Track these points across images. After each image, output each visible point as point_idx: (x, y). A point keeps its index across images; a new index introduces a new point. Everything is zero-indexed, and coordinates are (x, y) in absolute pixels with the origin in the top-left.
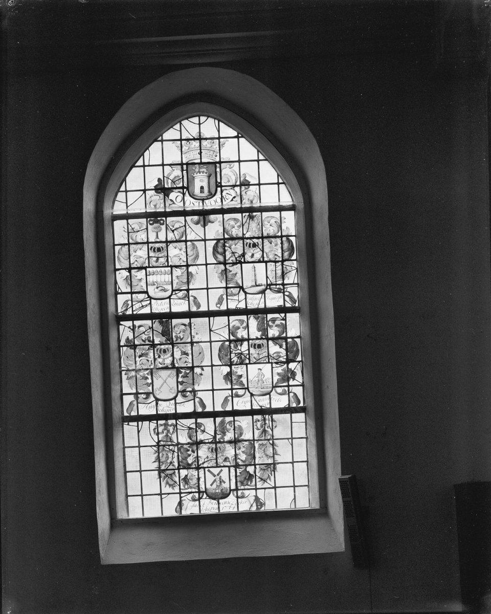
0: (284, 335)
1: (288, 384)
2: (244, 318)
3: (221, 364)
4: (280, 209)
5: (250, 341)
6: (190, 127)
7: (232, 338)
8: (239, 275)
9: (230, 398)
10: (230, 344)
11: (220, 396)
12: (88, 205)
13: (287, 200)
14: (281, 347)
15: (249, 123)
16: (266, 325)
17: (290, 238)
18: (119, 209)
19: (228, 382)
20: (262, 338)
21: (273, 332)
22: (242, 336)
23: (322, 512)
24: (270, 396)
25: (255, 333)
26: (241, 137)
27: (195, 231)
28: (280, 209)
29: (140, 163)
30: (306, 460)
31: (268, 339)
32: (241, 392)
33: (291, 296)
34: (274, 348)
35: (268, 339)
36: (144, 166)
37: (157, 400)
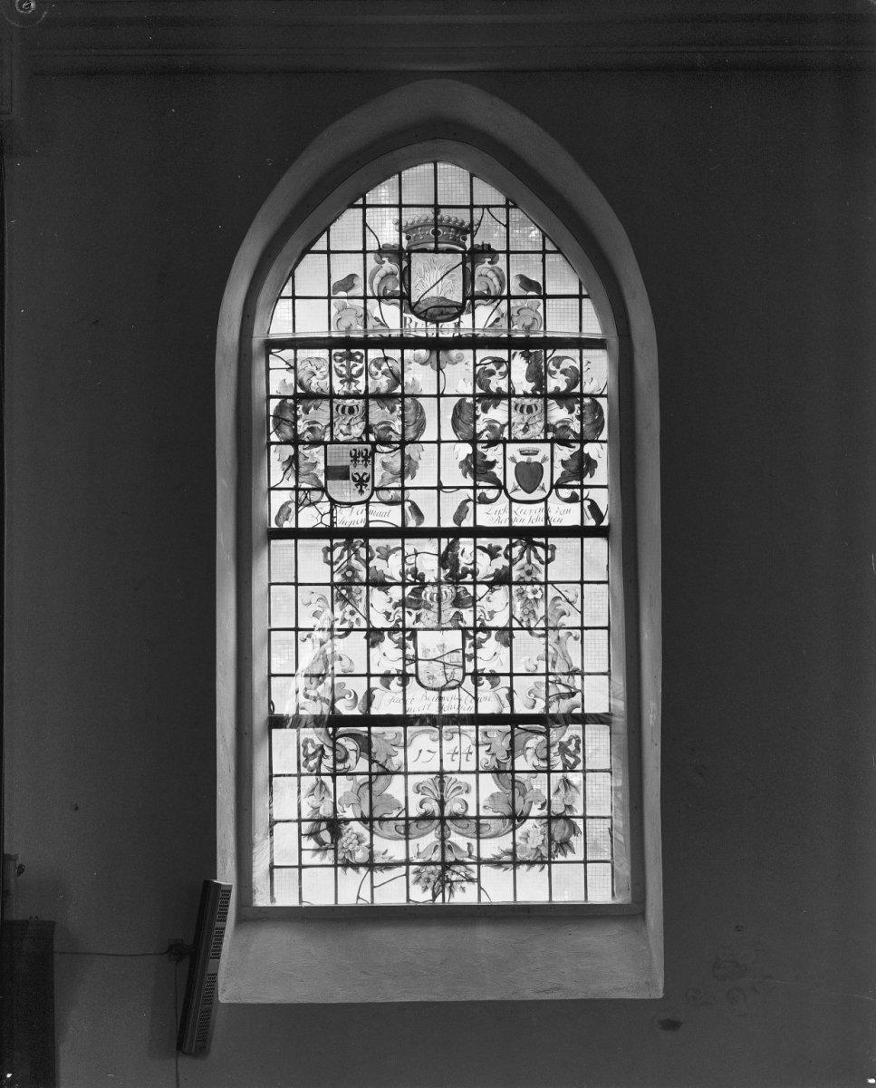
0: (577, 390)
1: (582, 482)
2: (503, 354)
3: (457, 439)
4: (581, 344)
5: (513, 399)
6: (417, 180)
7: (479, 391)
8: (500, 464)
9: (470, 505)
10: (475, 401)
11: (451, 502)
12: (228, 333)
13: (593, 328)
14: (571, 411)
15: (527, 185)
16: (543, 370)
17: (598, 399)
18: (280, 323)
19: (468, 475)
20: (533, 396)
21: (557, 382)
22: (499, 389)
23: (627, 914)
24: (546, 505)
25: (523, 384)
26: (512, 207)
27: (419, 376)
28: (581, 344)
29: (321, 244)
30: (606, 625)
31: (546, 396)
32: (491, 494)
33: (594, 507)
34: (558, 414)
35: (546, 396)
36: (329, 252)
37: (333, 502)
